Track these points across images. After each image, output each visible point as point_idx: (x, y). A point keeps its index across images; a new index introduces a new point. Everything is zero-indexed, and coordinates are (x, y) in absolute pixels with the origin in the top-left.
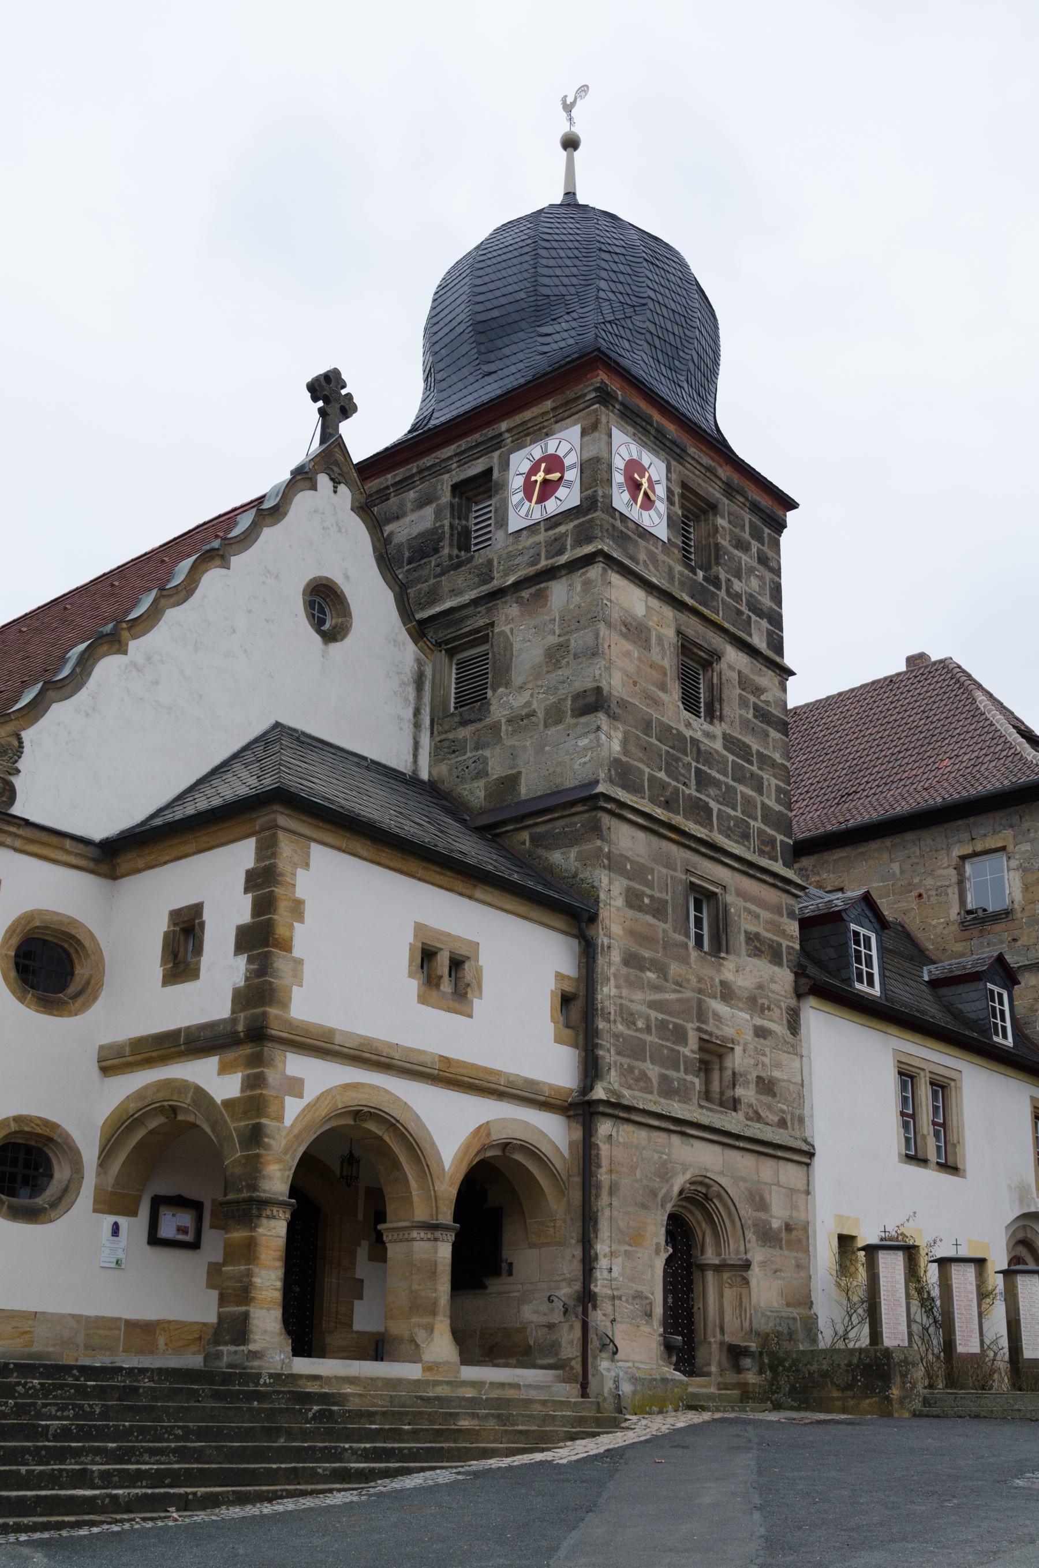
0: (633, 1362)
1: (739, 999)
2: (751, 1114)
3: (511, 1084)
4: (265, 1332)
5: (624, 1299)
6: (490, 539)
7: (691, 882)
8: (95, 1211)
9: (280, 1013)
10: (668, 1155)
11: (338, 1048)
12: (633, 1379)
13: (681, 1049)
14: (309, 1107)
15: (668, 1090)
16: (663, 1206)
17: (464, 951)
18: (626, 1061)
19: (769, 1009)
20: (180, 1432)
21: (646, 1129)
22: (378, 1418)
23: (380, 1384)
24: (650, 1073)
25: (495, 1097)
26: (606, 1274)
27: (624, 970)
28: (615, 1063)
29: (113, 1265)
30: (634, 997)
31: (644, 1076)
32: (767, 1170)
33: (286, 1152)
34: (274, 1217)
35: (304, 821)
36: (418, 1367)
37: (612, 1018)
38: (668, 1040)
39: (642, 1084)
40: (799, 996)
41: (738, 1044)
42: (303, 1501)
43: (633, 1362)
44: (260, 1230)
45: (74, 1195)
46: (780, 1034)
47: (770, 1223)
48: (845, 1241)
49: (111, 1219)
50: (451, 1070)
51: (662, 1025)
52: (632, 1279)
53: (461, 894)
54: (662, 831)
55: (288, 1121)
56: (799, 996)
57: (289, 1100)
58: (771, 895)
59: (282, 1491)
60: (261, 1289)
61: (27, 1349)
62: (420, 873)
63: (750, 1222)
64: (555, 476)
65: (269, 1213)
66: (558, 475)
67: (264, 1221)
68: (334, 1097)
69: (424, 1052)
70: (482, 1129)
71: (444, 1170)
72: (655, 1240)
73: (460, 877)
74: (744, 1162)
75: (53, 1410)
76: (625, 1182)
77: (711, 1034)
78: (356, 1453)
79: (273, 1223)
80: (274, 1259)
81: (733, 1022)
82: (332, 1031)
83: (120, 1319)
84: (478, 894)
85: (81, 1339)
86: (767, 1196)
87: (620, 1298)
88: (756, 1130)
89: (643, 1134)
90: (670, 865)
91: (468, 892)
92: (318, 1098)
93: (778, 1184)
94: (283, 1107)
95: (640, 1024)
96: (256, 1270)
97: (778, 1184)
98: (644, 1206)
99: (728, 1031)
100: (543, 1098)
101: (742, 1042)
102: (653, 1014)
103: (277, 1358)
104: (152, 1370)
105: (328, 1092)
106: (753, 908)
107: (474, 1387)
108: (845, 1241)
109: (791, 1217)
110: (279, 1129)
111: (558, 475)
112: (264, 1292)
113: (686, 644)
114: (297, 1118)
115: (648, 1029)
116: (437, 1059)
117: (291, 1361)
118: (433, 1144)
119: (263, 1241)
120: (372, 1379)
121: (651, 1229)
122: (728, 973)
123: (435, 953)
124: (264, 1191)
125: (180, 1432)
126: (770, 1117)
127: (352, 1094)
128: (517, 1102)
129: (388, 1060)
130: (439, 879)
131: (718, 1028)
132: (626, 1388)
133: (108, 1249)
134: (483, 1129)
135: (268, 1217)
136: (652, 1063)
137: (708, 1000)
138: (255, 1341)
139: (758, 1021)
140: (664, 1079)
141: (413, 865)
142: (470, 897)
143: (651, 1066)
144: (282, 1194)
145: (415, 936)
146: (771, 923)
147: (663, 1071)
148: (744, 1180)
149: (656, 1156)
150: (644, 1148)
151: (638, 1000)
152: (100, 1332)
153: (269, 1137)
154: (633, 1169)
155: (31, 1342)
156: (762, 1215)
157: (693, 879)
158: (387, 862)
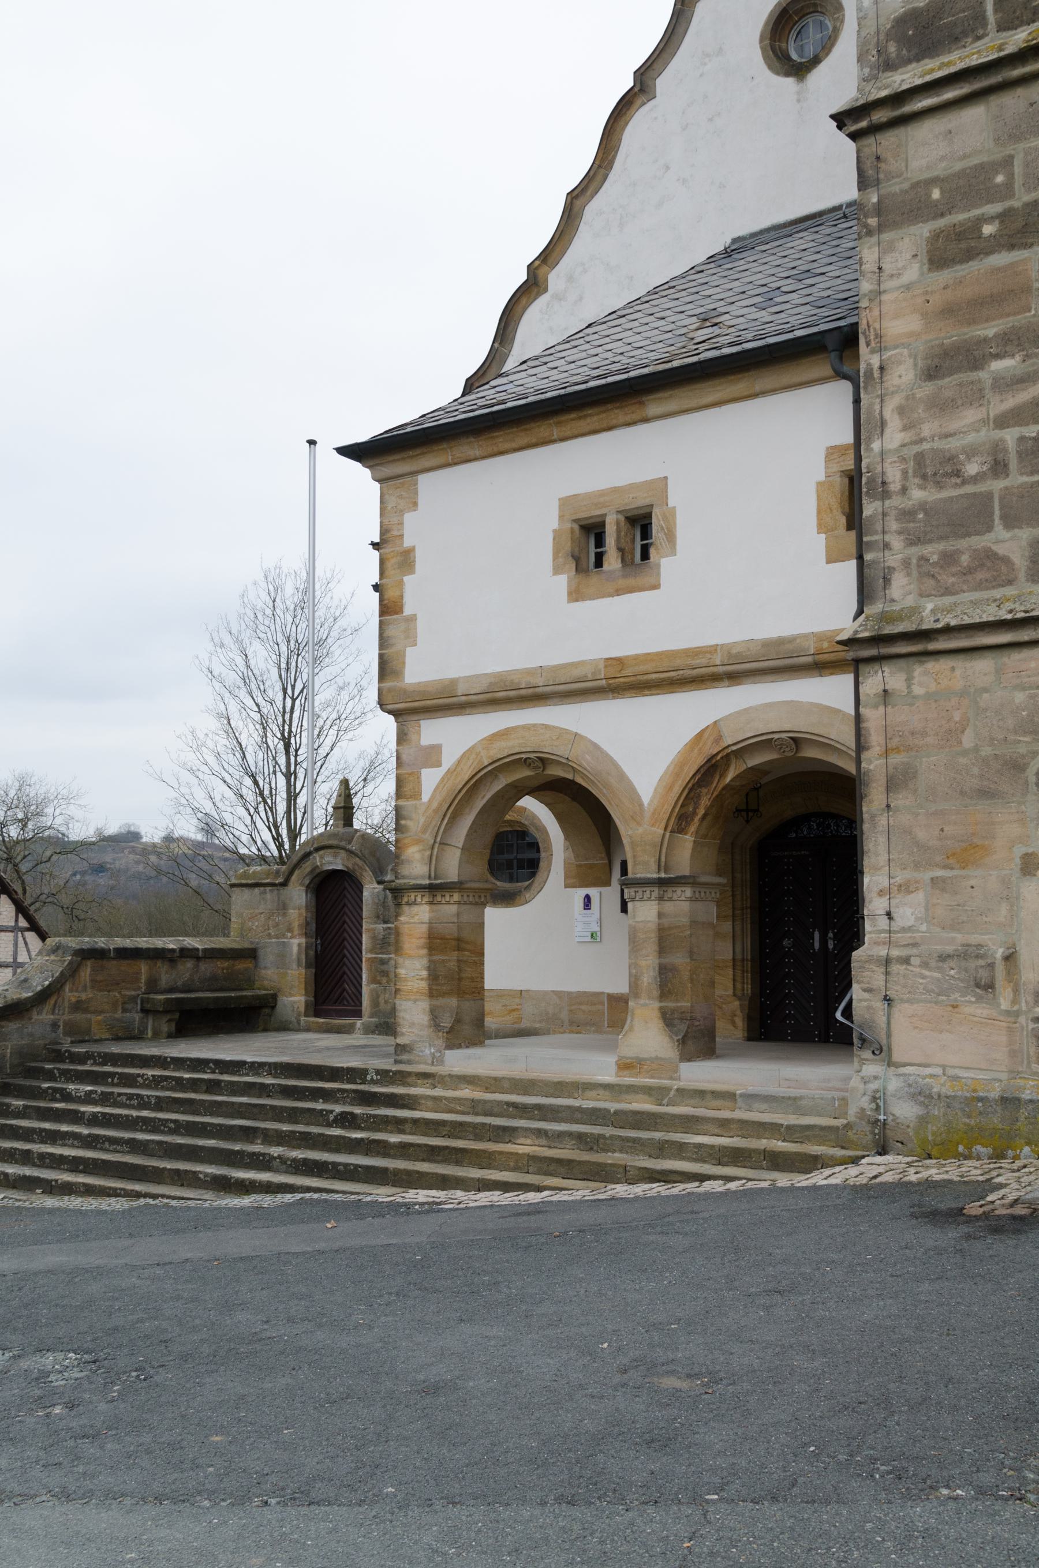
0: (944, 1067)
4: (412, 1025)
5: (915, 961)
8: (566, 886)
9: (395, 683)
11: (464, 698)
12: (921, 1095)
17: (637, 501)
20: (172, 1125)
21: (989, 654)
22: (408, 1127)
23: (506, 1085)
25: (727, 683)
26: (883, 923)
28: (906, 563)
29: (589, 939)
30: (954, 426)
31: (989, 558)
33: (424, 831)
34: (414, 903)
35: (394, 461)
36: (610, 1060)
37: (895, 487)
42: (93, 1202)
43: (944, 1067)
44: (402, 918)
45: (546, 873)
49: (582, 892)
50: (624, 673)
52: (955, 926)
53: (563, 439)
55: (425, 797)
57: (425, 773)
59: (121, 1189)
60: (406, 980)
61: (516, 1026)
62: (556, 433)
65: (405, 899)
67: (406, 908)
68: (477, 754)
69: (582, 663)
70: (706, 735)
71: (641, 805)
73: (610, 406)
75: (124, 1098)
78: (285, 1163)
79: (415, 909)
80: (418, 948)
82: (453, 682)
83: (603, 993)
84: (653, 409)
85: (564, 1015)
87: (906, 961)
89: (982, 667)
91: (635, 417)
92: (459, 762)
94: (419, 783)
95: (972, 469)
96: (400, 960)
98: (985, 794)
100: (809, 659)
102: (1010, 436)
103: (427, 1052)
104: (270, 1064)
105: (470, 750)
107: (650, 1095)
110: (416, 808)
112: (409, 983)
114: (435, 791)
115: (999, 467)
116: (601, 666)
117: (442, 1056)
118: (680, 764)
119: (405, 929)
120: (496, 1079)
123: (649, 516)
124: (404, 877)
125: (172, 1125)
128: (770, 677)
129: (530, 691)
130: (584, 425)
133: (583, 923)
135: (408, 904)
138: (403, 1034)
141: (543, 429)
142: (646, 420)
143: (1005, 534)
144: (423, 877)
145: (561, 517)
150: (986, 690)
151: (968, 428)
152: (583, 1007)
153: (405, 819)
154: (952, 735)
155: (520, 1019)
158: (507, 446)
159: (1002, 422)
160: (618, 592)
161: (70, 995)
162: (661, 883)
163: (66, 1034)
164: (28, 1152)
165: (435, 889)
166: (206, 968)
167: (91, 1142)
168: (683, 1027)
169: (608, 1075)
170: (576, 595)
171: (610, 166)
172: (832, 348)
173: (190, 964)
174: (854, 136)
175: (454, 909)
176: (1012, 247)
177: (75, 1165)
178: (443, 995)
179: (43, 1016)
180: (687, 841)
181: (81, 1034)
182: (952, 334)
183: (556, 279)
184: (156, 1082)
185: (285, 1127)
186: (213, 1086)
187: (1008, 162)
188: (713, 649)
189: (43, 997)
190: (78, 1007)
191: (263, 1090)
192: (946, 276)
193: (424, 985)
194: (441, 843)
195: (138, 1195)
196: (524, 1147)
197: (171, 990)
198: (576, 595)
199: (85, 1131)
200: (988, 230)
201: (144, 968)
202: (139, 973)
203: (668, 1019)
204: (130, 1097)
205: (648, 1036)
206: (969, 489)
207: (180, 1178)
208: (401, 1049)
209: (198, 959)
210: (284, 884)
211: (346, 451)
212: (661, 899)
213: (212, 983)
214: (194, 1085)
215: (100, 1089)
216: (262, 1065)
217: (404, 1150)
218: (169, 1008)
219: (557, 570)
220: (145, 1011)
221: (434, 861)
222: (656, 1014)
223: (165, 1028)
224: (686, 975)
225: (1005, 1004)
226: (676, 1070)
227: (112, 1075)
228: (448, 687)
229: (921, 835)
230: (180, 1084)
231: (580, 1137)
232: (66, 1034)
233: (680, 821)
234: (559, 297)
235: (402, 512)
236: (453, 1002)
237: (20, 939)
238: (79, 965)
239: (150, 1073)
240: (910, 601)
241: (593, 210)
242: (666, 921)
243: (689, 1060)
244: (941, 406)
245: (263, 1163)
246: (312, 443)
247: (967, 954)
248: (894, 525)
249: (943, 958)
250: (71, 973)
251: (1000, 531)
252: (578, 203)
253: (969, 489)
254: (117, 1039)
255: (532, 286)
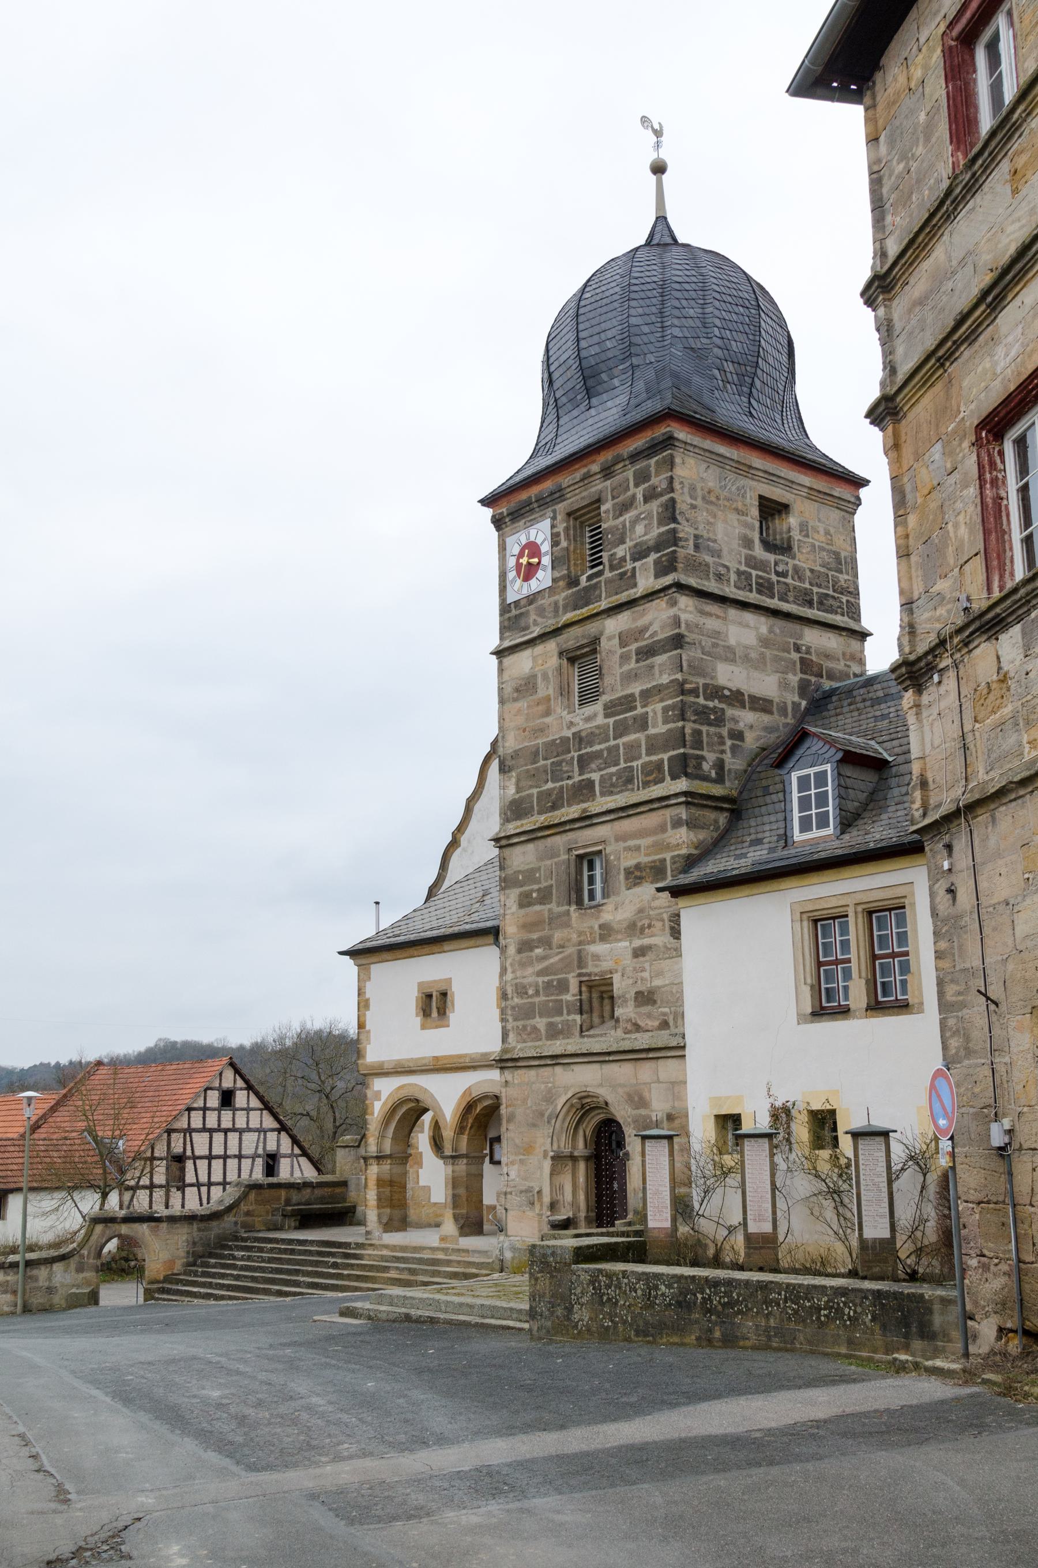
1: (618, 932)
2: (629, 1027)
3: (473, 1060)
6: (600, 545)
7: (577, 856)
10: (552, 1083)
12: (513, 1249)
13: (564, 997)
14: (384, 1104)
15: (554, 1033)
16: (549, 1122)
18: (520, 1023)
19: (650, 926)
24: (538, 1026)
27: (518, 958)
30: (526, 973)
31: (535, 1029)
32: (645, 1071)
37: (510, 996)
38: (552, 995)
39: (533, 1036)
40: (358, 1041)
41: (617, 972)
46: (661, 944)
47: (650, 1117)
48: (729, 1122)
51: (548, 985)
52: (525, 1179)
54: (540, 834)
56: (358, 1041)
57: (376, 1103)
58: (651, 820)
62: (416, 953)
63: (629, 1120)
64: (535, 560)
66: (536, 560)
69: (424, 1058)
72: (543, 1149)
74: (622, 1072)
76: (519, 1112)
77: (589, 975)
81: (612, 956)
82: (383, 1062)
84: (446, 948)
86: (646, 1094)
87: (511, 1193)
88: (642, 1040)
89: (532, 1072)
90: (553, 854)
93: (658, 1081)
95: (530, 992)
97: (658, 1081)
98: (534, 1125)
99: (606, 965)
101: (620, 969)
102: (540, 980)
106: (631, 843)
108: (729, 1122)
109: (673, 1107)
111: (536, 560)
113: (570, 655)
115: (537, 993)
118: (459, 1104)
121: (540, 1141)
122: (607, 916)
126: (650, 1023)
127: (402, 1091)
131: (597, 966)
132: (508, 1255)
134: (468, 1091)
136: (540, 1017)
137: (587, 947)
139: (637, 943)
140: (550, 1025)
146: (655, 845)
147: (550, 1020)
148: (620, 1085)
149: (543, 1086)
154: (524, 1101)
156: (643, 1112)
157: (577, 853)
159: (539, 974)
160: (437, 1027)
161: (243, 1207)
162: (452, 1157)
163: (242, 1227)
164: (211, 1283)
165: (379, 1158)
166: (318, 1192)
167: (237, 1278)
168: (462, 1222)
169: (436, 1244)
170: (423, 1027)
171: (483, 788)
172: (493, 933)
173: (309, 1190)
174: (500, 847)
175: (388, 1167)
176: (541, 904)
177: (229, 1287)
178: (383, 1207)
179: (230, 1219)
180: (465, 1138)
181: (249, 1227)
182: (527, 936)
183: (464, 840)
184: (272, 1250)
185: (310, 1269)
186: (292, 1252)
187: (539, 869)
188: (465, 1056)
189: (230, 1209)
190: (248, 1213)
191: (310, 1253)
192: (523, 911)
193: (375, 1203)
194: (382, 1136)
195: (247, 1299)
196: (393, 1274)
197: (298, 1204)
198: (423, 1027)
199: (235, 1273)
200: (534, 895)
201: (283, 1193)
202: (281, 1195)
203: (456, 1218)
204: (258, 1257)
205: (449, 1227)
206: (530, 1000)
207: (267, 1292)
208: (368, 1233)
209: (314, 1187)
210: (358, 1146)
211: (341, 953)
212: (453, 1164)
213: (322, 1200)
214: (285, 1251)
215: (247, 1254)
216: (314, 1241)
217: (349, 1277)
218: (294, 1214)
219: (417, 1015)
220: (284, 1216)
221: (379, 1144)
222: (451, 1216)
223: (293, 1224)
224: (464, 1199)
225: (537, 1211)
226: (458, 1241)
227: (254, 1247)
228: (381, 1065)
229: (517, 1141)
230: (281, 1251)
231: (409, 1269)
232: (242, 1227)
233: (461, 1129)
234: (465, 850)
235: (365, 981)
236: (388, 1211)
237: (295, 1162)
238: (248, 1193)
239: (269, 1246)
240: (514, 1044)
241: (478, 807)
242: (456, 1174)
243: (466, 1235)
244: (523, 965)
245: (297, 1284)
246: (377, 903)
247: (529, 1190)
248: (509, 1012)
249: (521, 1192)
250: (244, 1196)
251: (538, 1019)
252: (471, 804)
253: (530, 1000)
254: (269, 1230)
255: (454, 844)
